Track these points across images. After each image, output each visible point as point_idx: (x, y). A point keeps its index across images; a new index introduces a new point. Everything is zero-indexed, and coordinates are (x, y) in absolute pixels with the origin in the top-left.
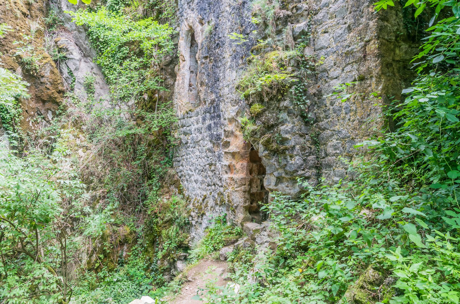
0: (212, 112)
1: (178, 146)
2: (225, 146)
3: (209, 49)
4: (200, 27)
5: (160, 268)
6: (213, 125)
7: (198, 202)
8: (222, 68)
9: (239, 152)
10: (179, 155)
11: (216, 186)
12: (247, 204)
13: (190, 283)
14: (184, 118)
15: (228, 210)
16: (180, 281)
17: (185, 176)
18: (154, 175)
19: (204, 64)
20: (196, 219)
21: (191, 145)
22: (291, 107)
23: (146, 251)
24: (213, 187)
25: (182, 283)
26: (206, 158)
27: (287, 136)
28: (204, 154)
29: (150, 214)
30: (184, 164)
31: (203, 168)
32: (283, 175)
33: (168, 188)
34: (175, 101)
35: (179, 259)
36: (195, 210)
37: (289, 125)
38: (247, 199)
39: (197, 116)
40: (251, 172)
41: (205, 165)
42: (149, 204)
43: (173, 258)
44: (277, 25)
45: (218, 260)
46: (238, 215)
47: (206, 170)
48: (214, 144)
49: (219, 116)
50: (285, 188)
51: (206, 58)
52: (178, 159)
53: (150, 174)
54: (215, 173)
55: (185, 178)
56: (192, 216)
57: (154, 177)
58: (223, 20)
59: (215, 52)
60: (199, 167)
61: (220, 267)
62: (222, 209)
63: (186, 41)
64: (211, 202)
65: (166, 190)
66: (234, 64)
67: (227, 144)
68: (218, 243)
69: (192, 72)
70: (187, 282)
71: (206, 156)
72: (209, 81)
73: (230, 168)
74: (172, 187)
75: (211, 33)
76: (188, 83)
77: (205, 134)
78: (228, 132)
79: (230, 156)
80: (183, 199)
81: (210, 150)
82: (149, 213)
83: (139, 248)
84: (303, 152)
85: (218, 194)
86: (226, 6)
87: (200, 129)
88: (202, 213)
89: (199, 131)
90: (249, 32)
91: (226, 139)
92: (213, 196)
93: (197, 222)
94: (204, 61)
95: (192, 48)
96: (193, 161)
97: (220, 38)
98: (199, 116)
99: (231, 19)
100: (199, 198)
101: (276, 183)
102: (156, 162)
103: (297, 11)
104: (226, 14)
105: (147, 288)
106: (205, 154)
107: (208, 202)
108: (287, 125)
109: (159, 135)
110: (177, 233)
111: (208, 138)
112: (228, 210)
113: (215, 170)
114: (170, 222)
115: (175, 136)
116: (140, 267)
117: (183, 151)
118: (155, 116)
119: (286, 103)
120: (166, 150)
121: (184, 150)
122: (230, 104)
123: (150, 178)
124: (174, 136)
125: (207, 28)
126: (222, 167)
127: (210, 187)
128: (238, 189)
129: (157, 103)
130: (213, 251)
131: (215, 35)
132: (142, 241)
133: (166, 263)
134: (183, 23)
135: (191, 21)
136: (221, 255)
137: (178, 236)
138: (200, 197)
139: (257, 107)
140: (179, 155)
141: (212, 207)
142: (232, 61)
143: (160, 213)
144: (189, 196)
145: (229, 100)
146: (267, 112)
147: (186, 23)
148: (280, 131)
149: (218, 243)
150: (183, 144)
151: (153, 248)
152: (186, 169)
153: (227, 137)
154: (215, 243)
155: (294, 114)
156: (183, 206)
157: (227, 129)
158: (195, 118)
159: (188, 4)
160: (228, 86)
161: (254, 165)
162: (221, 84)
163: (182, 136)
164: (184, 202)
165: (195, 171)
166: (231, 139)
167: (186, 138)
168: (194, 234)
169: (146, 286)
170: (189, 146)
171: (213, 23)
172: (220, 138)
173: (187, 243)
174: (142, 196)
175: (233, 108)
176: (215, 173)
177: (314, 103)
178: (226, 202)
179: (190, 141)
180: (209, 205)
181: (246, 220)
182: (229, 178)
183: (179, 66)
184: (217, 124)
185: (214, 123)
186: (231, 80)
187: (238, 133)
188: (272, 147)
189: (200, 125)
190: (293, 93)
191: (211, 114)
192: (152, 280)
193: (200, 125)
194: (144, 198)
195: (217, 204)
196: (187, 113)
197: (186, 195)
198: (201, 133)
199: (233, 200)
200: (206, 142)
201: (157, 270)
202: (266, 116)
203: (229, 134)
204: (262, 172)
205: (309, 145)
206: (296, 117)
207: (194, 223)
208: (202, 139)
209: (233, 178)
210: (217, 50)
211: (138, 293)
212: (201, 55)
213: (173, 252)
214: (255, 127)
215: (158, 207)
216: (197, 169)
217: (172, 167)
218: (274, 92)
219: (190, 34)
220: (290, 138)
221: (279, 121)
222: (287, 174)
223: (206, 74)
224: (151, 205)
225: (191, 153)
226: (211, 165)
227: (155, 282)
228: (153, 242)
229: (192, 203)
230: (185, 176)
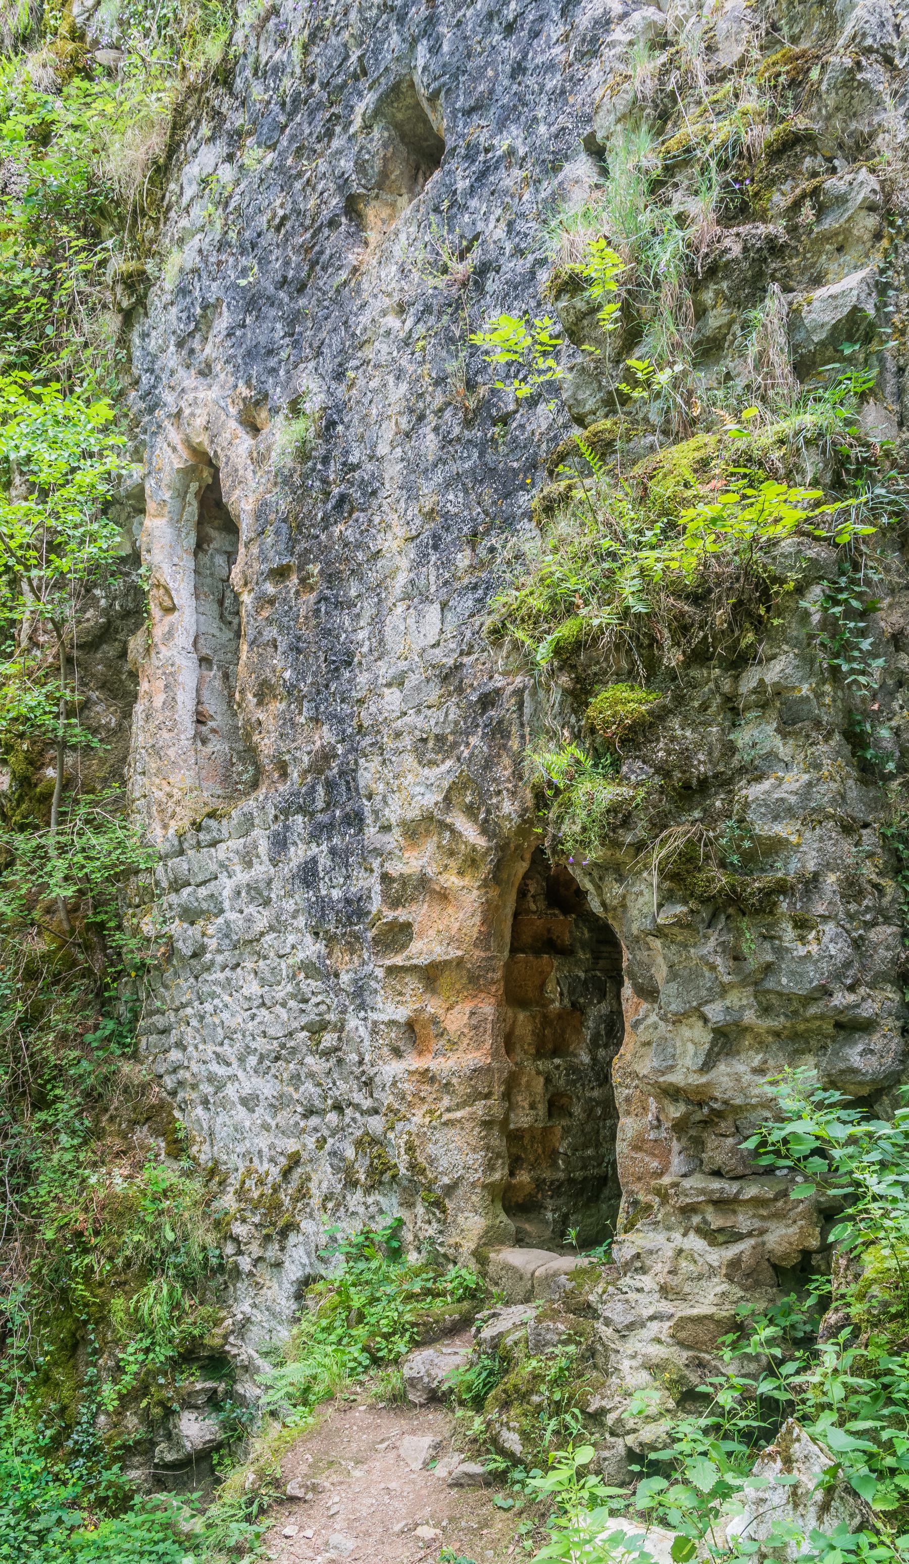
0: (320, 805)
1: (157, 967)
2: (387, 946)
3: (296, 528)
4: (245, 443)
5: (109, 1441)
6: (324, 861)
7: (261, 1182)
8: (368, 608)
9: (460, 962)
10: (164, 1002)
11: (349, 1111)
12: (497, 1176)
13: (295, 1508)
14: (182, 852)
15: (410, 1205)
16: (250, 1503)
17: (194, 1087)
18: (58, 1092)
19: (271, 602)
20: (255, 1249)
21: (220, 959)
22: (805, 689)
23: (46, 1380)
24: (332, 1117)
25: (262, 1511)
26: (292, 1003)
27: (783, 830)
28: (283, 990)
29: (54, 1242)
30: (188, 1040)
31: (283, 1046)
32: (749, 1017)
33: (125, 1137)
34: (138, 785)
35: (187, 1405)
36: (248, 1214)
37: (789, 777)
38: (498, 1155)
39: (246, 834)
40: (509, 1042)
41: (291, 1034)
42: (45, 1204)
43: (161, 1403)
44: (701, 313)
45: (397, 1401)
46: (460, 1219)
47: (294, 1051)
48: (331, 940)
49: (356, 820)
50: (747, 1078)
51: (280, 574)
52: (159, 1021)
53: (43, 1086)
54: (340, 1061)
55: (194, 1095)
56: (236, 1240)
57: (58, 1098)
58: (364, 382)
59: (330, 537)
60: (261, 1044)
61: (413, 1432)
62: (377, 1203)
63: (176, 521)
64: (323, 1178)
65: (118, 1144)
66: (431, 576)
67: (398, 935)
68: (386, 1336)
69: (204, 661)
70: (280, 1502)
71: (293, 996)
72: (301, 675)
73: (413, 1033)
74: (141, 1134)
75: (303, 454)
76: (191, 705)
77: (289, 905)
78: (404, 880)
79: (412, 983)
80: (188, 1174)
81: (310, 969)
82: (50, 1235)
83: (16, 1373)
84: (853, 907)
85: (359, 1144)
86: (384, 313)
87: (262, 885)
88: (281, 1224)
89: (258, 894)
90: (512, 407)
91: (390, 915)
92: (333, 1154)
93: (260, 1259)
94: (270, 588)
95: (205, 559)
96: (233, 1023)
97: (354, 468)
98: (256, 832)
99: (411, 368)
100: (266, 1166)
101: (708, 1055)
102: (63, 1038)
103: (819, 220)
104: (385, 349)
105: (60, 1521)
106: (289, 988)
107: (309, 1179)
108: (781, 780)
109: (72, 931)
110: (177, 1306)
111: (301, 922)
112: (410, 1205)
113: (337, 1049)
114: (150, 1268)
115: (145, 928)
116: (22, 1443)
117: (183, 988)
118: (51, 841)
119: (778, 669)
120: (107, 987)
121: (185, 983)
122: (410, 760)
123: (41, 1103)
124: (136, 930)
125: (283, 435)
126: (374, 1032)
127: (314, 1121)
128: (458, 1115)
129: (54, 800)
130: (366, 1367)
131: (326, 460)
132: (24, 1344)
133: (131, 1421)
134: (160, 439)
135: (200, 422)
136: (412, 1382)
137: (179, 1319)
138: (272, 1160)
139: (622, 700)
140: (164, 1002)
141: (327, 1199)
142: (422, 559)
143: (97, 1233)
144: (216, 1162)
145: (407, 741)
146: (675, 723)
147: (175, 436)
148: (747, 805)
149: (386, 1336)
150: (182, 958)
151: (75, 1367)
152: (198, 1057)
153: (395, 903)
154: (373, 1334)
155: (818, 724)
156: (195, 1203)
157: (395, 868)
158: (236, 844)
159: (180, 345)
160: (399, 681)
161: (521, 1016)
162: (363, 679)
163: (176, 928)
164: (195, 1187)
165: (242, 1060)
166: (415, 913)
167: (194, 931)
168: (246, 1307)
169: (55, 1516)
170: (212, 962)
171: (312, 405)
172: (362, 914)
173: (218, 1341)
174: (11, 1174)
175: (426, 771)
176: (340, 1061)
177: (890, 682)
178: (403, 1171)
179: (212, 944)
180: (314, 1191)
181: (492, 1238)
182: (411, 1073)
183: (149, 634)
184: (348, 852)
185: (333, 851)
186: (416, 648)
187: (452, 880)
188: (710, 880)
189: (261, 869)
190: (816, 618)
191: (312, 815)
192: (78, 1489)
193: (263, 868)
194: (22, 1180)
195: (352, 1184)
196: (198, 827)
197: (203, 1158)
198: (267, 903)
199: (432, 1161)
200: (291, 939)
201: (95, 1450)
202: (673, 739)
203: (400, 891)
204: (550, 1046)
205: (873, 876)
206: (827, 738)
207: (245, 1263)
208: (272, 928)
209: (435, 1072)
210: (337, 530)
211: (25, 1541)
212: (256, 566)
213: (162, 1381)
214: (625, 791)
215: (86, 1210)
216: (249, 1051)
217: (134, 1056)
218: (720, 616)
219: (194, 487)
220: (794, 839)
221: (735, 762)
222: (766, 1010)
223: (282, 646)
224: (54, 1205)
225: (218, 990)
226: (317, 1029)
227: (92, 1496)
228: (73, 1347)
229: (231, 1189)
230: (194, 1087)
